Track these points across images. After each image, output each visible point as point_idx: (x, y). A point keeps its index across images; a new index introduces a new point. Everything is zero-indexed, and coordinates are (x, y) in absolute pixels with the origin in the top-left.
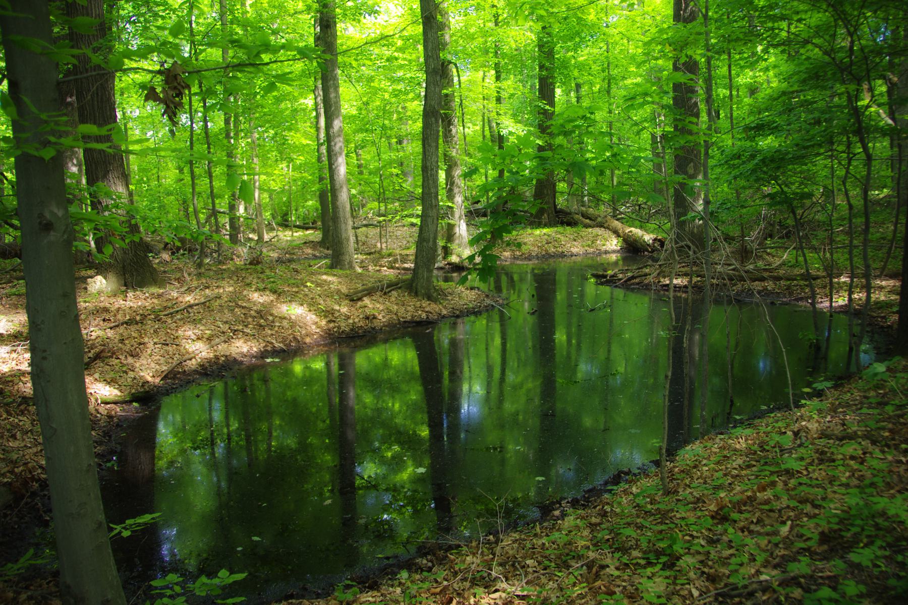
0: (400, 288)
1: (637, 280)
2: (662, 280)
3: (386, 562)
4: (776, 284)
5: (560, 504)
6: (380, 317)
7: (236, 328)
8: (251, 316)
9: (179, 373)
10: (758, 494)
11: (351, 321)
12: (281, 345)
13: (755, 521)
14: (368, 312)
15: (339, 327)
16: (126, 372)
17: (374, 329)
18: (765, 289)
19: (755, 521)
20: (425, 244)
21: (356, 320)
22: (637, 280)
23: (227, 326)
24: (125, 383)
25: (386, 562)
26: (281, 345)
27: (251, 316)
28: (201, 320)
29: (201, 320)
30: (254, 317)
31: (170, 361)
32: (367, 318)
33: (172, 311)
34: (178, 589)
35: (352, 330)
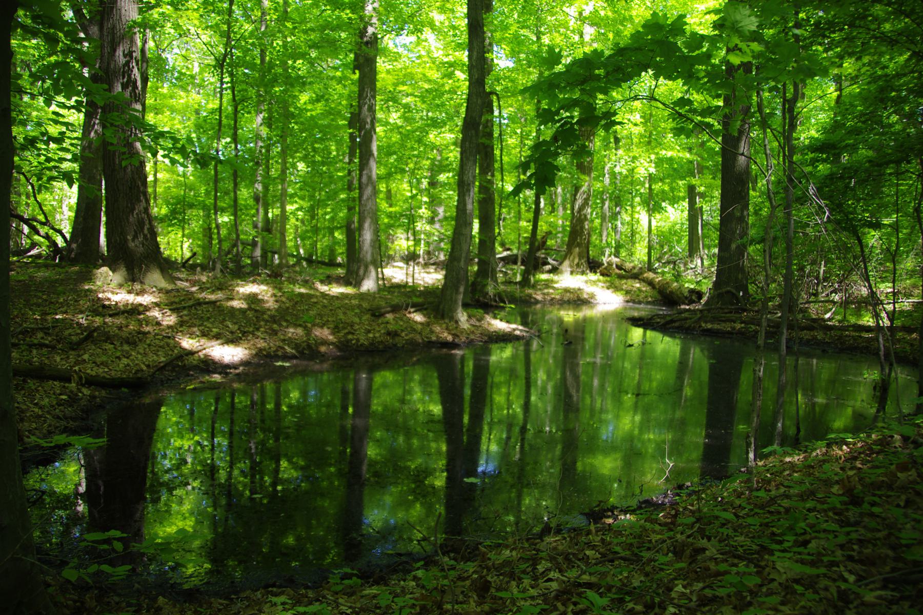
0: (426, 309)
1: (677, 324)
2: (703, 325)
3: (397, 559)
4: (826, 334)
5: (613, 512)
6: (403, 334)
7: (246, 329)
8: (263, 320)
9: (178, 366)
10: (899, 475)
11: (371, 335)
12: (294, 351)
13: (902, 504)
14: (391, 327)
15: (358, 340)
16: (118, 358)
17: (395, 345)
18: (814, 338)
19: (902, 504)
20: (456, 263)
21: (377, 335)
22: (677, 324)
23: (236, 327)
24: (117, 369)
25: (397, 559)
26: (294, 351)
27: (263, 320)
28: (209, 318)
29: (209, 318)
30: (267, 321)
31: (170, 353)
32: (389, 333)
33: (178, 306)
34: (119, 546)
35: (372, 344)
